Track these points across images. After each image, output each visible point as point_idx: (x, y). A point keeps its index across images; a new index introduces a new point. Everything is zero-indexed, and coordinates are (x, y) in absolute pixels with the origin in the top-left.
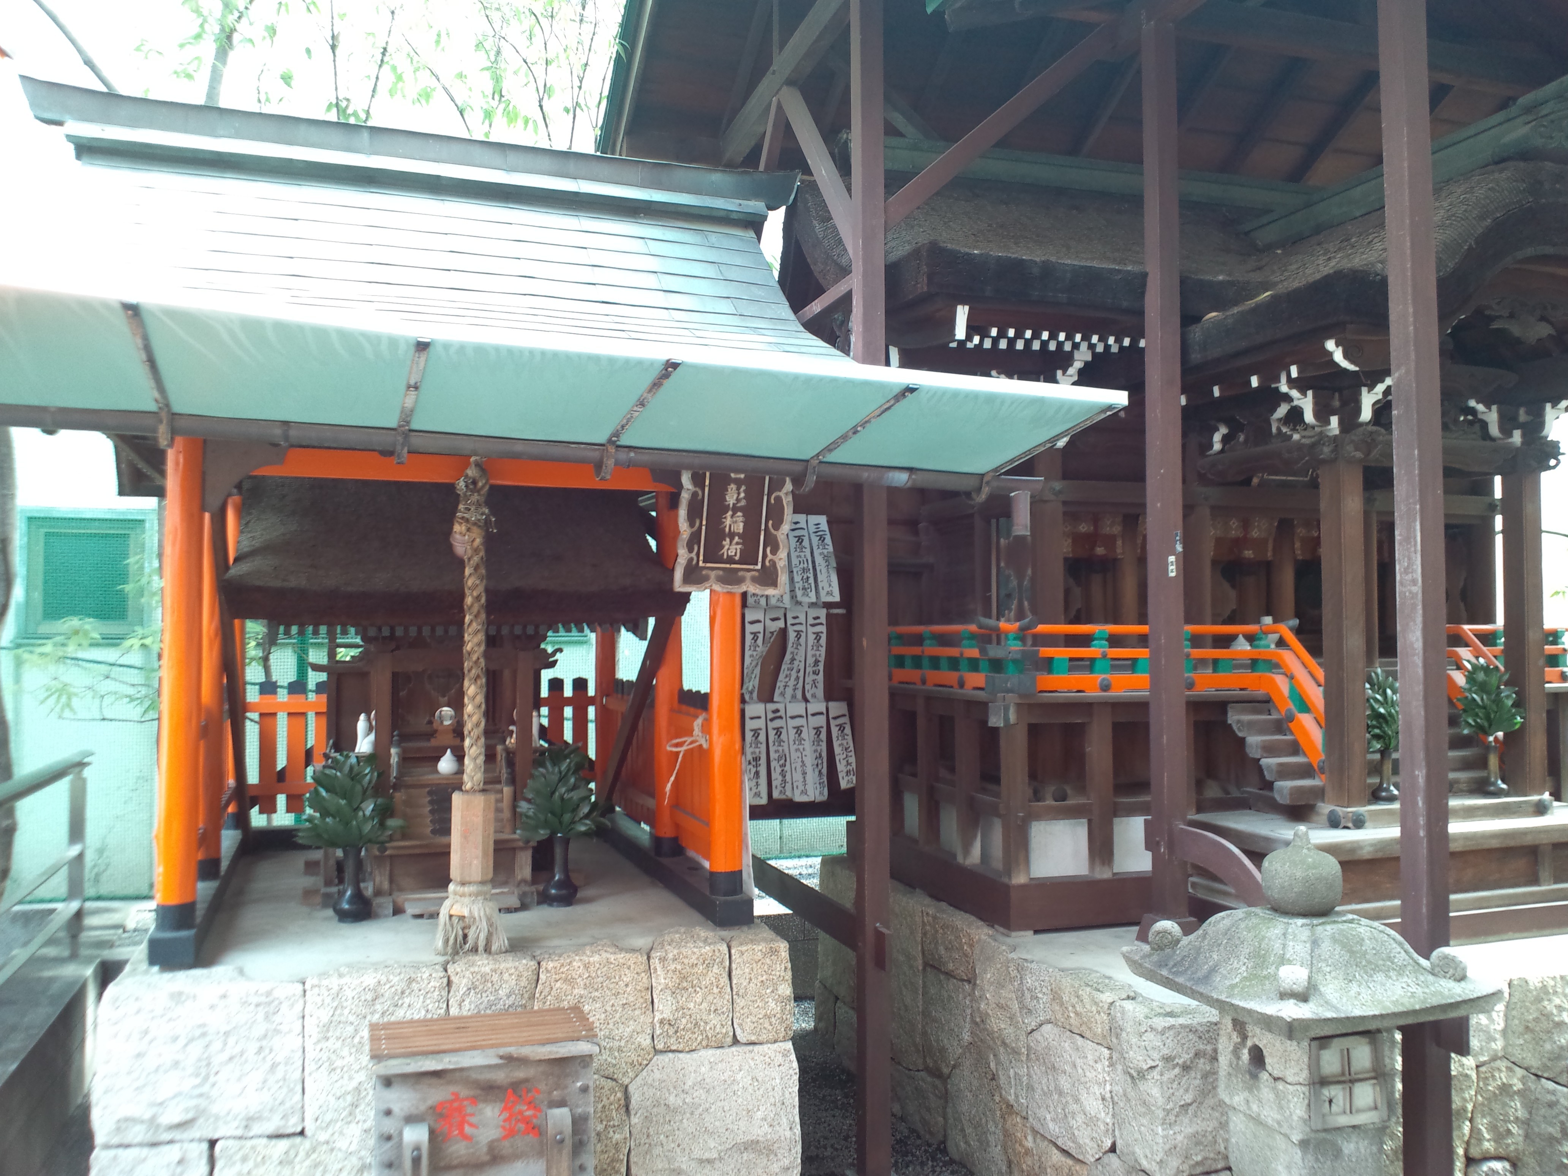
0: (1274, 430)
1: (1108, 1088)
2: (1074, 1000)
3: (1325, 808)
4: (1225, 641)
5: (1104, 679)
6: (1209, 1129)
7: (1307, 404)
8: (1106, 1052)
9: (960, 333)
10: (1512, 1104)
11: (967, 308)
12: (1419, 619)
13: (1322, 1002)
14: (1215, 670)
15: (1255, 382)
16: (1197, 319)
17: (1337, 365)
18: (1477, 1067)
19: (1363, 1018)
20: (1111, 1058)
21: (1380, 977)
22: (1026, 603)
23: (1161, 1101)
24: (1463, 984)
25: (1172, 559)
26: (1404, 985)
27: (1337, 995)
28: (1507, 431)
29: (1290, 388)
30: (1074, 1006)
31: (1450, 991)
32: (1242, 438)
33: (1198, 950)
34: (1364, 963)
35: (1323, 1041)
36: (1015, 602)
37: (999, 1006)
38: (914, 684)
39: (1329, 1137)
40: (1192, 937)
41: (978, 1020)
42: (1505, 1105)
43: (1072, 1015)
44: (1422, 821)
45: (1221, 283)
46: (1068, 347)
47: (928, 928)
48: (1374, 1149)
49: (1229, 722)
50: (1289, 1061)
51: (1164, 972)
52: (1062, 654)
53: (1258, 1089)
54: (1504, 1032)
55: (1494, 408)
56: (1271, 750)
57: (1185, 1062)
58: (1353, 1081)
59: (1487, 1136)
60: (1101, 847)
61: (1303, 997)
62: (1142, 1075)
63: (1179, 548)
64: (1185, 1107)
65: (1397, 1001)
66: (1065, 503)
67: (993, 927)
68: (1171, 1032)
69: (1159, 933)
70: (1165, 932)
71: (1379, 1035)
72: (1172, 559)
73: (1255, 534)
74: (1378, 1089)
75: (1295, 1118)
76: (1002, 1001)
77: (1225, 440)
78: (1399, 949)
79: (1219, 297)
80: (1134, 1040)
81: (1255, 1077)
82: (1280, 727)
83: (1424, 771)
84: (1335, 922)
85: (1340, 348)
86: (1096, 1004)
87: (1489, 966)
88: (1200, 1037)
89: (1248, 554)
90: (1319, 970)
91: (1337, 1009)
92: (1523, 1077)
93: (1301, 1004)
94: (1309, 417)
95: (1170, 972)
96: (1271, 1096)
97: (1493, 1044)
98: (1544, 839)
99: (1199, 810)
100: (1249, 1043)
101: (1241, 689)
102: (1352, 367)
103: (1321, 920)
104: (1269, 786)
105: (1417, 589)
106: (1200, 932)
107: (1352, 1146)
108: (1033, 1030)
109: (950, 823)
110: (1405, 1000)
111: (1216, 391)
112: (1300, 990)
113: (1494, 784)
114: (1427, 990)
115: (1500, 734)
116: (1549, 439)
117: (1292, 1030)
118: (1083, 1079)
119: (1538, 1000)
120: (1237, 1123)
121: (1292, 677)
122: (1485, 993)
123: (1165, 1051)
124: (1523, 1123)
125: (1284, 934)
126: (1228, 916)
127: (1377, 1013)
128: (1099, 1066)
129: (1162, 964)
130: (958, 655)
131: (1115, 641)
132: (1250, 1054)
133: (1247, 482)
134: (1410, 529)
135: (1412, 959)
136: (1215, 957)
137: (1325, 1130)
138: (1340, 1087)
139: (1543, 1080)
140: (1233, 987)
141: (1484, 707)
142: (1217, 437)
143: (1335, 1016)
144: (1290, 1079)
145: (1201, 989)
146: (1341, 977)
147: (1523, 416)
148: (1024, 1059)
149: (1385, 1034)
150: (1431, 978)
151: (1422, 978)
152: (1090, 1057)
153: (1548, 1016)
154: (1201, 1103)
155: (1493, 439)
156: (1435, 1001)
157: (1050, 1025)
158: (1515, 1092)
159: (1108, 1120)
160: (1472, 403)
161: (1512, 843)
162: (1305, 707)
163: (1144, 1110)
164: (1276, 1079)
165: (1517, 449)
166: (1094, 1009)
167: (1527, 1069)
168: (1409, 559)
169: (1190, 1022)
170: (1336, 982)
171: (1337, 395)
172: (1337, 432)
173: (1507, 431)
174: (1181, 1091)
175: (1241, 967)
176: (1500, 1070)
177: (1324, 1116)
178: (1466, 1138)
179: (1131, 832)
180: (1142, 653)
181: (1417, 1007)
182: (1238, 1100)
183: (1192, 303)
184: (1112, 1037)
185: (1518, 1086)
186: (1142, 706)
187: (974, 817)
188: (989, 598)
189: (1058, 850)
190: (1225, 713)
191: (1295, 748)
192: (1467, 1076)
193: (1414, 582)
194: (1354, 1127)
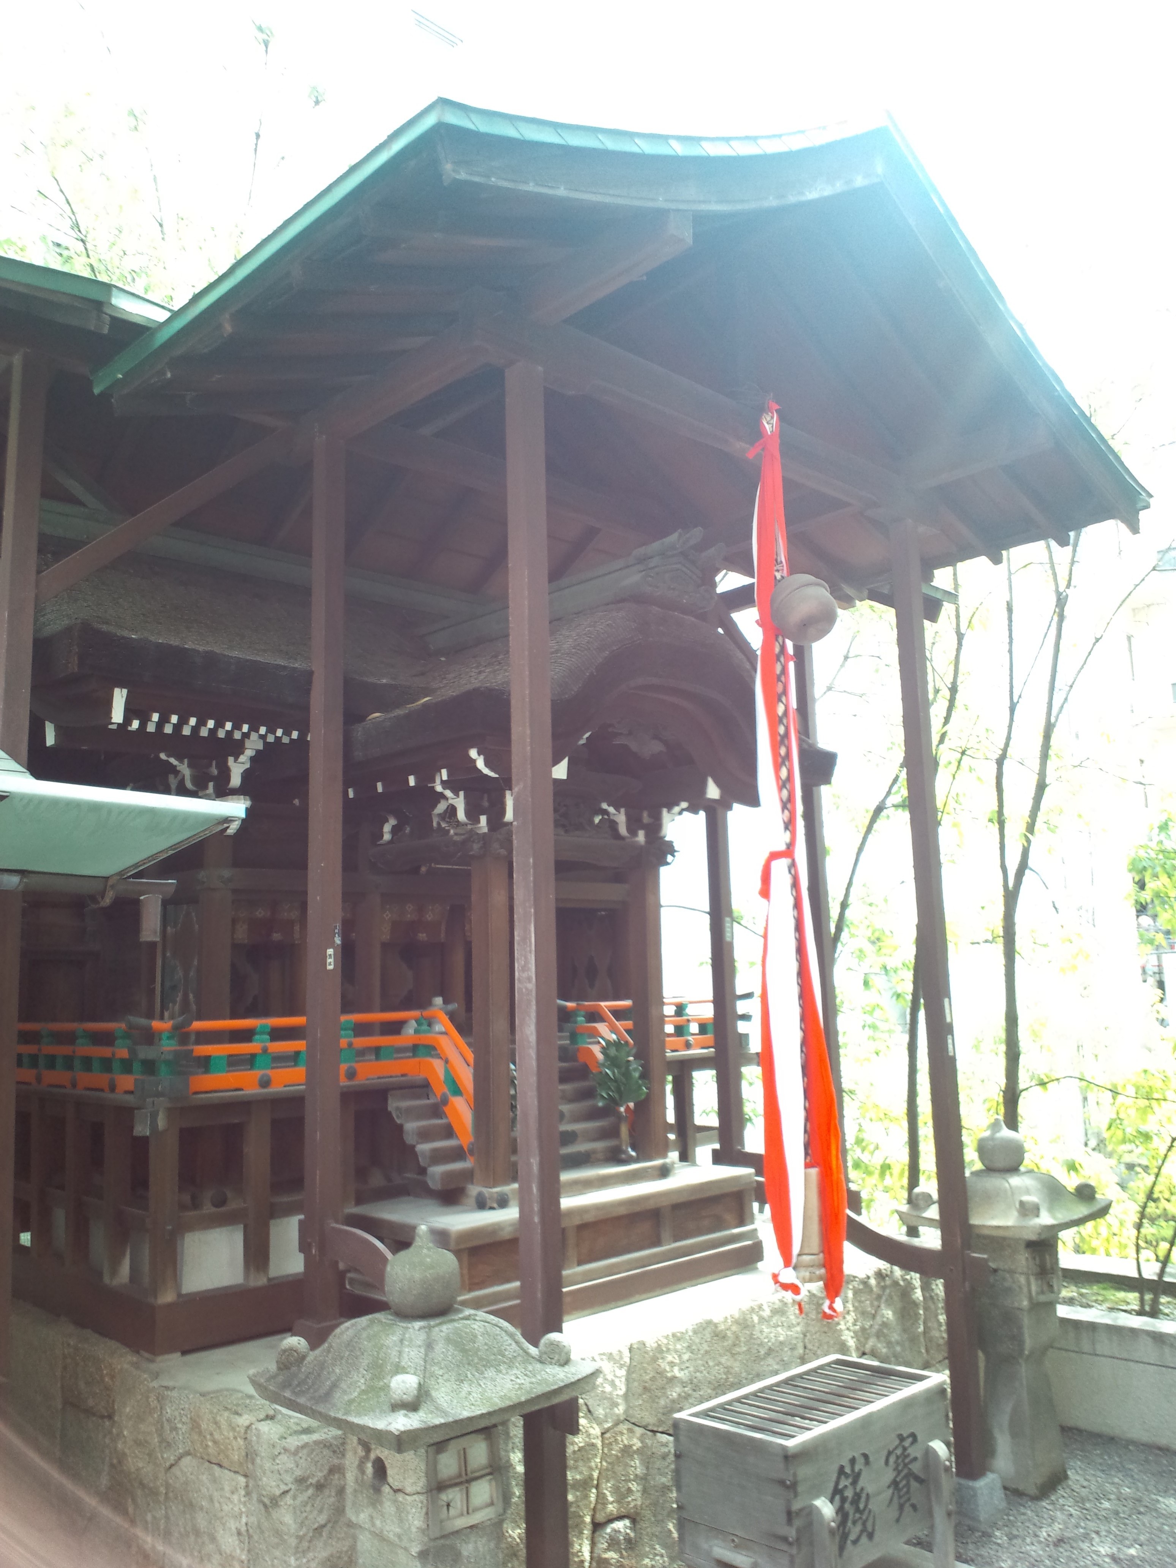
0: (435, 824)
1: (244, 1520)
2: (212, 1427)
3: (474, 1190)
4: (395, 1028)
5: (263, 1076)
6: (345, 1549)
7: (460, 803)
8: (242, 1480)
9: (117, 715)
10: (632, 1463)
11: (125, 691)
12: (533, 1014)
13: (432, 1408)
14: (378, 1058)
15: (412, 781)
16: (362, 718)
17: (480, 771)
18: (603, 1434)
19: (470, 1419)
20: (247, 1486)
21: (490, 1373)
22: (191, 996)
23: (293, 1527)
24: (566, 1368)
25: (330, 951)
26: (513, 1378)
27: (448, 1398)
28: (633, 831)
29: (444, 789)
30: (211, 1434)
31: (556, 1376)
32: (408, 830)
33: (322, 1366)
34: (476, 1361)
35: (440, 1446)
36: (180, 995)
37: (139, 1443)
38: (65, 1087)
39: (448, 1542)
40: (318, 1352)
41: (115, 1461)
42: (627, 1465)
43: (210, 1444)
44: (536, 1207)
45: (385, 685)
46: (237, 735)
47: (69, 1361)
48: (492, 1545)
49: (389, 1109)
50: (408, 1472)
51: (287, 1394)
52: (218, 1051)
53: (381, 1503)
54: (626, 1396)
55: (623, 810)
56: (425, 1135)
57: (318, 1481)
58: (469, 1481)
59: (611, 1499)
60: (257, 1253)
61: (412, 1406)
62: (275, 1502)
63: (338, 941)
64: (319, 1530)
65: (505, 1395)
66: (235, 891)
67: (138, 1352)
68: (305, 1451)
69: (285, 1351)
70: (292, 1350)
71: (495, 1429)
72: (330, 951)
73: (429, 917)
74: (494, 1483)
75: (414, 1530)
76: (141, 1437)
77: (395, 830)
78: (510, 1341)
79: (383, 699)
80: (267, 1465)
81: (377, 1490)
82: (436, 1111)
83: (538, 1159)
84: (454, 1320)
85: (482, 757)
86: (233, 1429)
87: (598, 1342)
88: (334, 1452)
89: (422, 936)
90: (432, 1375)
91: (445, 1413)
92: (642, 1435)
93: (411, 1414)
94: (461, 815)
95: (294, 1392)
96: (393, 1509)
97: (616, 1409)
98: (666, 1202)
99: (359, 1201)
100: (373, 1456)
101: (402, 1075)
102: (492, 774)
103: (438, 1321)
104: (423, 1171)
105: (532, 986)
106: (326, 1345)
107: (471, 1547)
108: (171, 1466)
109: (99, 1239)
110: (512, 1394)
111: (380, 788)
112: (410, 1399)
113: (626, 1152)
114: (533, 1380)
115: (631, 1105)
116: (667, 839)
117: (402, 1442)
118: (220, 1514)
119: (655, 1359)
120: (365, 1542)
121: (447, 1061)
122: (584, 1375)
123: (298, 1473)
124: (642, 1479)
125: (401, 1341)
126: (353, 1325)
127: (484, 1411)
128: (235, 1498)
129: (285, 1385)
130: (109, 1055)
131: (277, 1034)
132: (373, 1466)
133: (416, 870)
134: (526, 930)
135: (522, 1349)
136: (337, 1371)
137: (443, 1537)
138: (457, 1489)
139: (659, 1435)
140: (351, 1402)
141: (616, 1081)
142: (387, 828)
143: (443, 1421)
144: (409, 1490)
145: (321, 1408)
146: (453, 1379)
147: (646, 818)
148: (162, 1498)
149: (500, 1428)
150: (538, 1366)
151: (530, 1368)
152: (227, 1488)
153: (661, 1373)
154: (336, 1522)
155: (622, 838)
156: (540, 1390)
157: (189, 1458)
158: (635, 1452)
159: (244, 1557)
160: (604, 806)
161: (637, 1209)
162: (458, 1091)
163: (276, 1540)
164: (397, 1491)
165: (641, 847)
166: (231, 1435)
167: (645, 1427)
168: (526, 958)
169: (324, 1436)
170: (448, 1384)
171: (486, 796)
172: (486, 830)
173: (633, 831)
174: (315, 1512)
175: (360, 1380)
176: (622, 1433)
177: (442, 1521)
178: (592, 1506)
179: (287, 1233)
180: (299, 1045)
181: (523, 1399)
182: (363, 1518)
183: (355, 703)
184: (247, 1465)
185: (637, 1444)
186: (295, 1102)
187: (123, 1232)
188: (153, 991)
189: (213, 1260)
190: (385, 1100)
191: (448, 1132)
192: (593, 1445)
193: (529, 979)
194: (471, 1527)
